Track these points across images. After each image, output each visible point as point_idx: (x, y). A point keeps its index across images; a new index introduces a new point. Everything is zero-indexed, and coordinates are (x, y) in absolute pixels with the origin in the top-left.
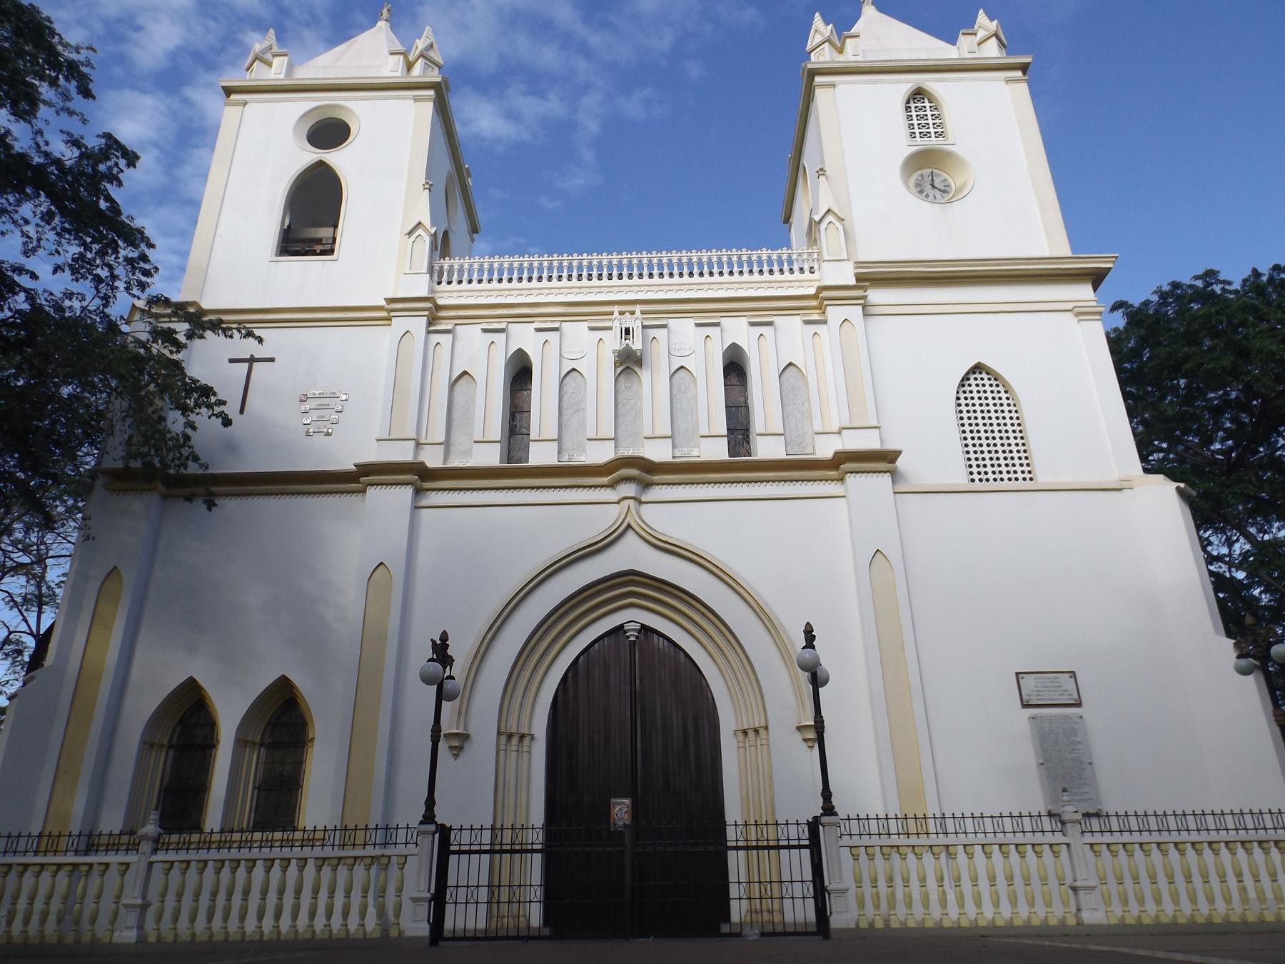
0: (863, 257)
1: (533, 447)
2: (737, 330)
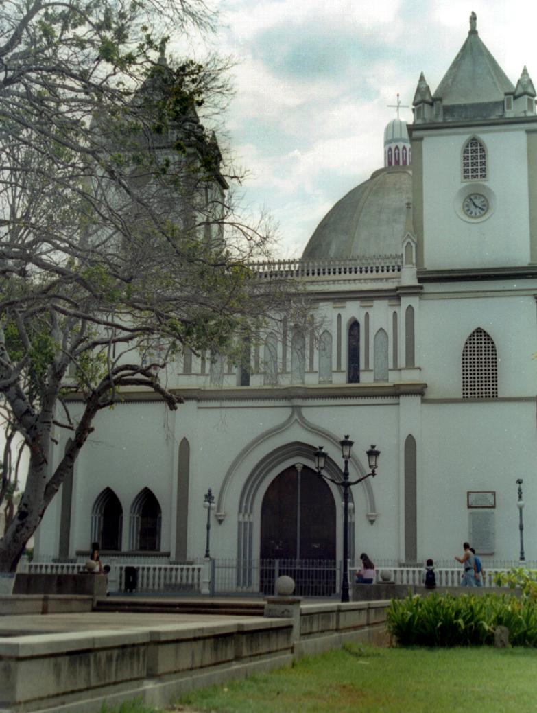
2: (353, 310)
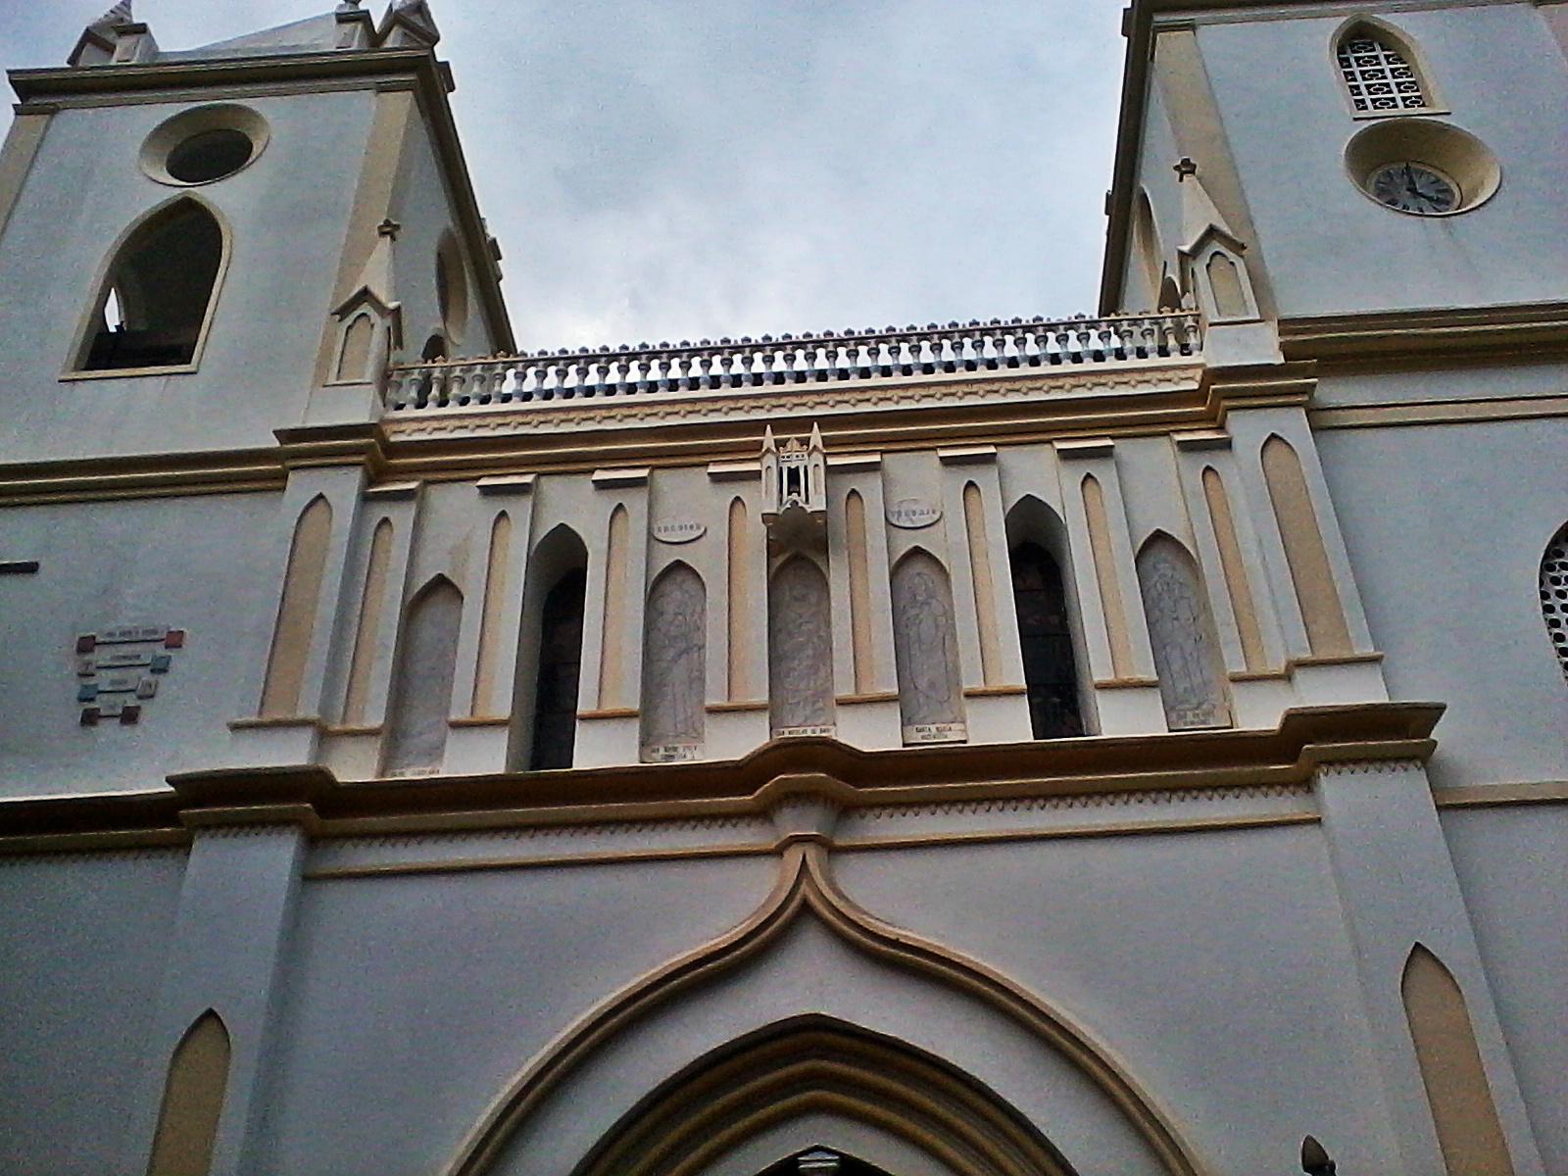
0: (1287, 314)
1: (583, 735)
2: (1036, 472)
